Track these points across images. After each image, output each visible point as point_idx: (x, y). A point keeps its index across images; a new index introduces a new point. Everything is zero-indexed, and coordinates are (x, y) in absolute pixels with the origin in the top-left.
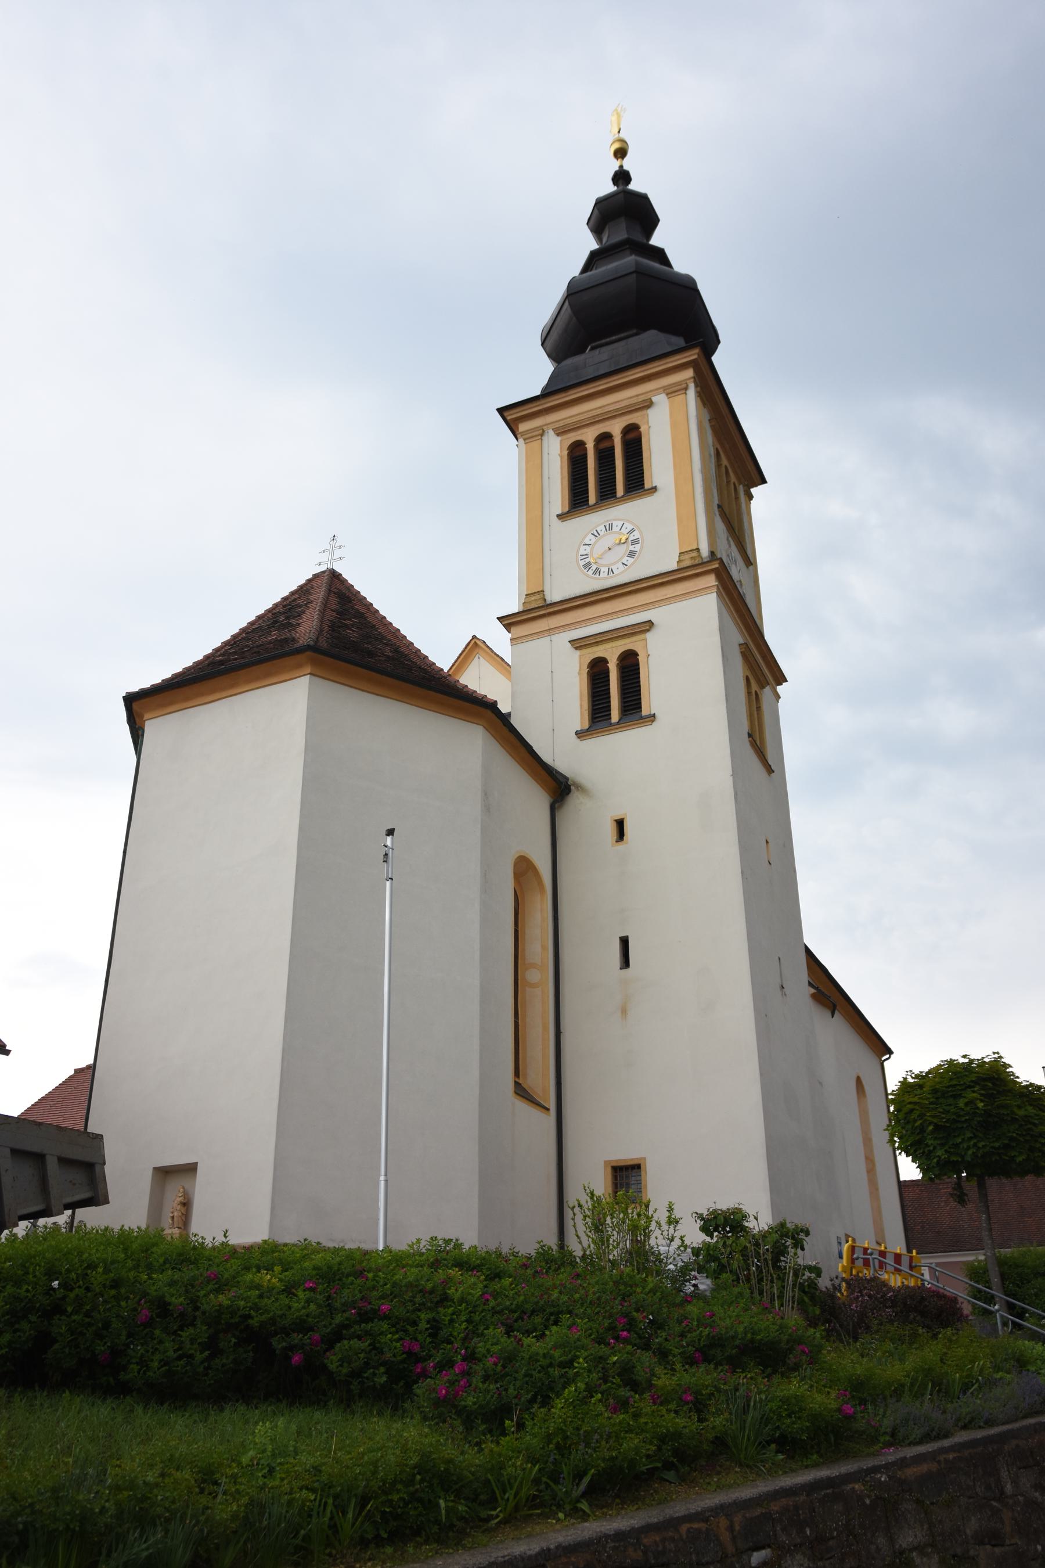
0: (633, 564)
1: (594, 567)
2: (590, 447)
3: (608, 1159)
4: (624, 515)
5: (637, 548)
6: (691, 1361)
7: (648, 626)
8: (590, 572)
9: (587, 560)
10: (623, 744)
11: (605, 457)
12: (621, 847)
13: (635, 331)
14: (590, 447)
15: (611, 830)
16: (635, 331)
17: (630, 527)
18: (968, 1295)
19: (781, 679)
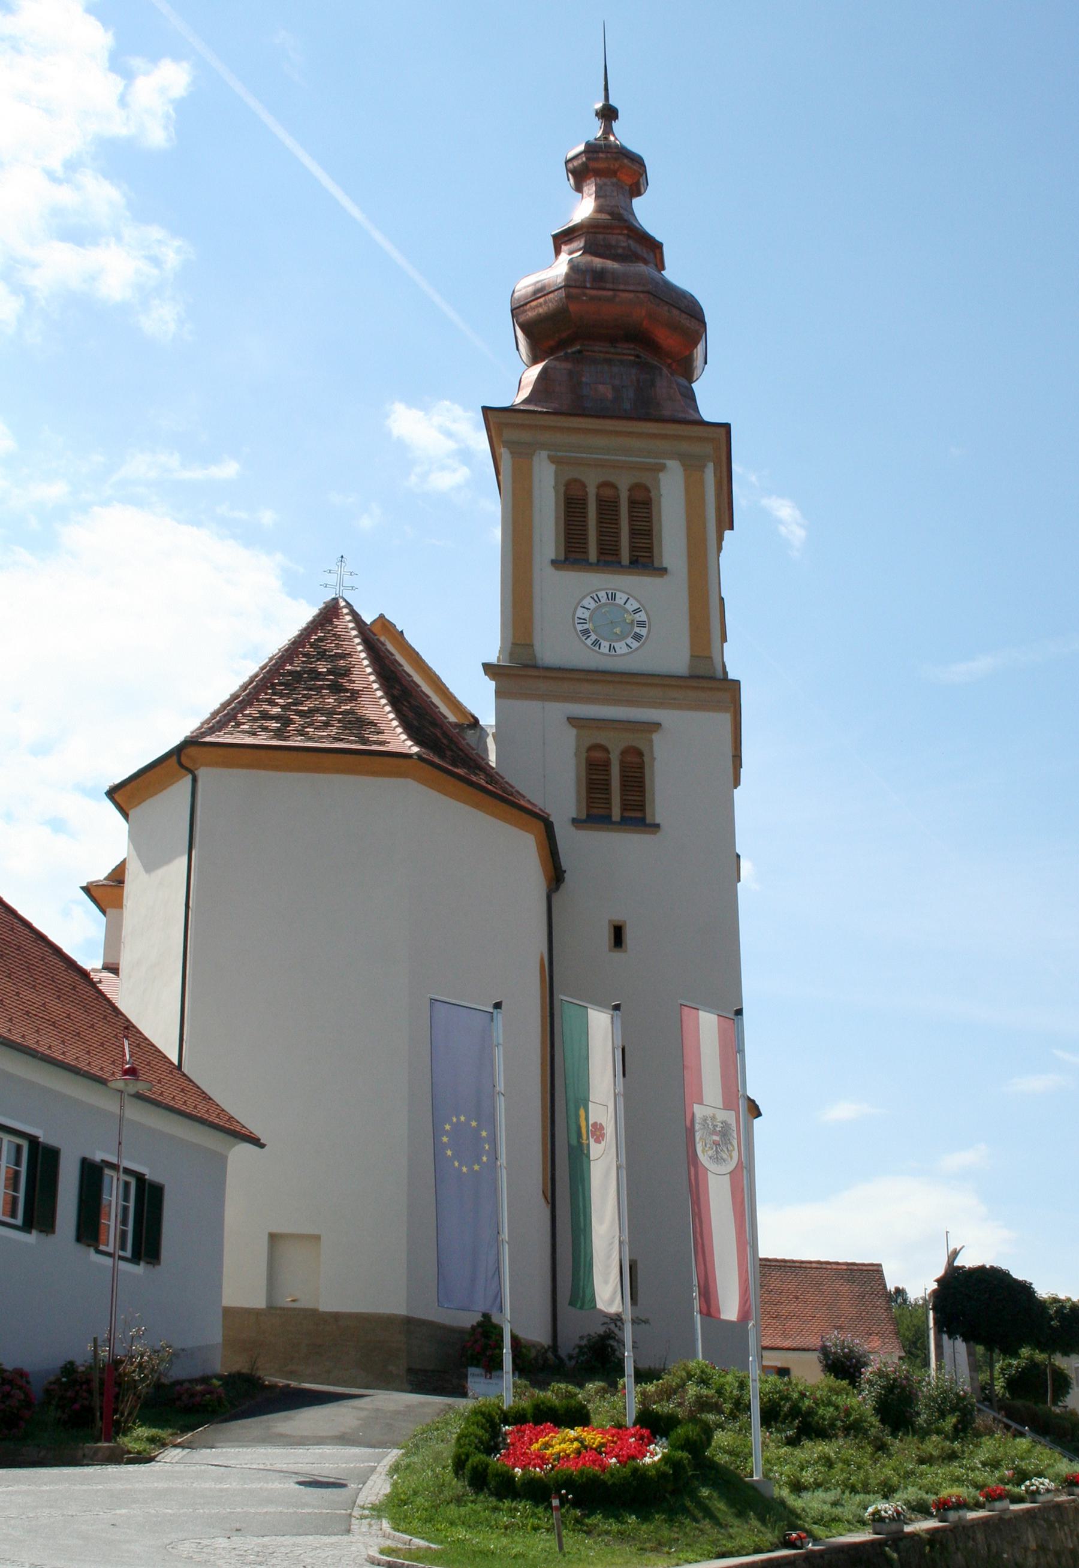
0: (637, 649)
1: (593, 637)
2: (592, 491)
3: (87, 1156)
4: (628, 590)
5: (643, 632)
6: (100, 1379)
7: (656, 726)
8: (589, 642)
9: (586, 626)
10: (625, 845)
11: (608, 508)
12: (617, 955)
13: (708, 1023)
14: (592, 491)
15: (606, 936)
16: (708, 1023)
17: (636, 605)
18: (763, 1394)
19: (731, 528)
